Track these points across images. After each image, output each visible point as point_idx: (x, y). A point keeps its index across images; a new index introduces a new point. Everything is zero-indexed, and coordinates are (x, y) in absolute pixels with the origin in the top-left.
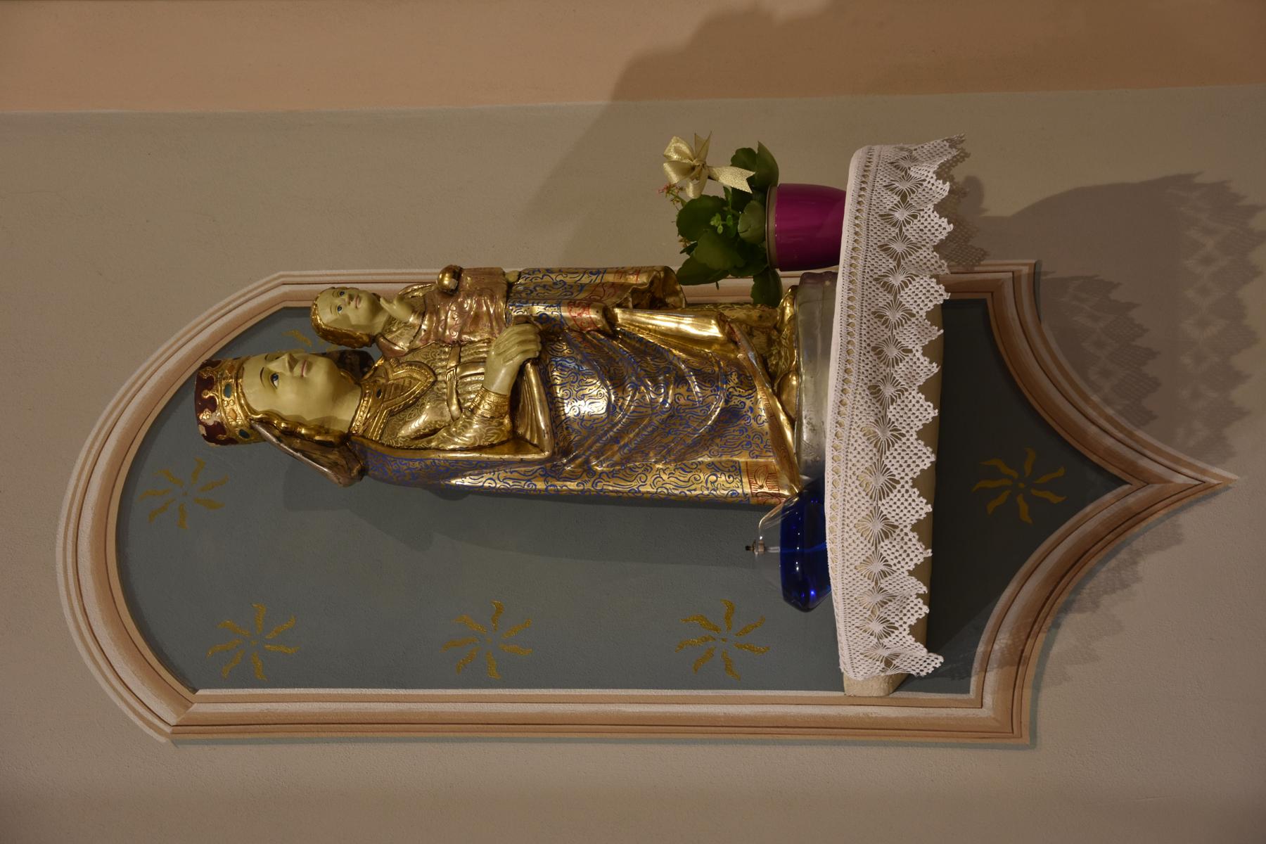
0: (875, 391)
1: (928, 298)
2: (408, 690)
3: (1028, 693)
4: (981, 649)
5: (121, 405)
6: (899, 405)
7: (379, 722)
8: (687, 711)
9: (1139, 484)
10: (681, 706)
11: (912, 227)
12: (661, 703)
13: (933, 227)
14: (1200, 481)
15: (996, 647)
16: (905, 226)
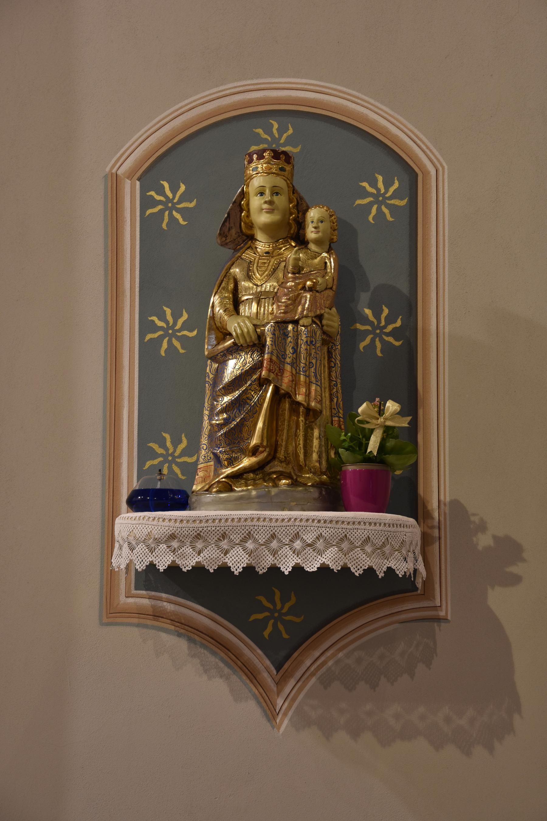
0: (173, 537)
1: (235, 562)
2: (138, 293)
3: (136, 621)
4: (164, 595)
5: (341, 94)
6: (166, 550)
7: (118, 280)
8: (124, 443)
9: (277, 678)
10: (127, 439)
11: (288, 551)
12: (129, 428)
13: (288, 563)
14: (279, 712)
15: (165, 604)
16: (289, 547)
